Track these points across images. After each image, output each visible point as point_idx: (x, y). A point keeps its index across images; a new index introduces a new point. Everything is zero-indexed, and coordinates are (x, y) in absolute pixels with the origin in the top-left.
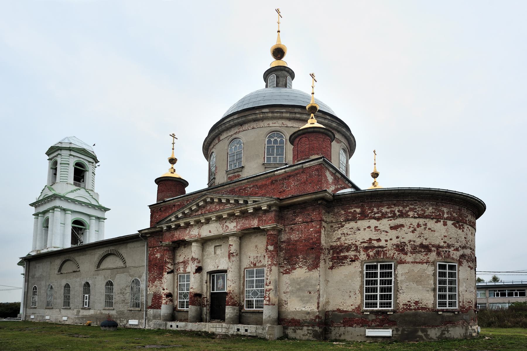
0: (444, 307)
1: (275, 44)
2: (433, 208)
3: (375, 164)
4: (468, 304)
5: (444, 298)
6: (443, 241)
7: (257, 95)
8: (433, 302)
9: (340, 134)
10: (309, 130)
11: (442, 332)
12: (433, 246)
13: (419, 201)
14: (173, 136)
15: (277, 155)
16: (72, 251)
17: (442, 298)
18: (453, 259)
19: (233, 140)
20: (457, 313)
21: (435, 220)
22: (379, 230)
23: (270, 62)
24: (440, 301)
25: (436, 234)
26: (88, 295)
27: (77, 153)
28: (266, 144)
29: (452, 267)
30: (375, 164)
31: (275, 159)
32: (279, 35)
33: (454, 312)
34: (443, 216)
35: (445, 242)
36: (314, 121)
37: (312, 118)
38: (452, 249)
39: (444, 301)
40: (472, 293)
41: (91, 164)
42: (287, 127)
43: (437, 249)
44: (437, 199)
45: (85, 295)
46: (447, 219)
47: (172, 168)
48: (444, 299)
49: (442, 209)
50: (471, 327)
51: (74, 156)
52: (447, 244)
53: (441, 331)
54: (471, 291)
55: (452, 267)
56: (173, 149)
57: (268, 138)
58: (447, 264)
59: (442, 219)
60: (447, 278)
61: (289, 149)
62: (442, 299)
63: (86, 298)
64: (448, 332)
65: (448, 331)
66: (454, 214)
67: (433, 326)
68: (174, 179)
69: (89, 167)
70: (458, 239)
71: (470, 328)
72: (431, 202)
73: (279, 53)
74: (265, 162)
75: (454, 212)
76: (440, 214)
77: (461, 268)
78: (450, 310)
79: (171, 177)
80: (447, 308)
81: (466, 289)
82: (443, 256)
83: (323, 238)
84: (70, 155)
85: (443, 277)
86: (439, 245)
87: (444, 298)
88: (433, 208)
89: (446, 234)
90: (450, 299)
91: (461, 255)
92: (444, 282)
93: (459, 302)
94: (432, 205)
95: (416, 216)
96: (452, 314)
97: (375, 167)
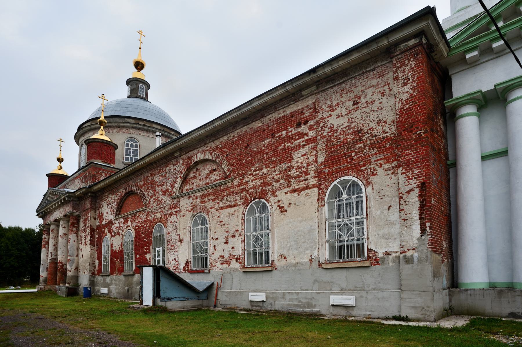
7: (119, 104)
14: (61, 140)
15: (133, 156)
16: (504, 28)
22: (190, 211)
26: (161, 249)
31: (132, 159)
32: (140, 51)
45: (157, 249)
63: (159, 254)
73: (139, 66)
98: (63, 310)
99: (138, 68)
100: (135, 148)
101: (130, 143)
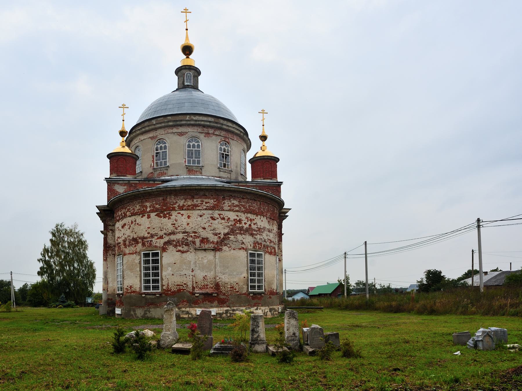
0: (157, 290)
2: (139, 206)
3: (263, 125)
5: (157, 282)
6: (147, 232)
7: (164, 102)
8: (139, 286)
9: (184, 127)
10: (119, 154)
11: (145, 312)
12: (140, 238)
13: (131, 202)
17: (156, 282)
18: (156, 247)
20: (158, 295)
21: (141, 215)
25: (142, 227)
29: (156, 254)
30: (263, 125)
33: (155, 295)
34: (146, 210)
35: (148, 233)
38: (156, 237)
39: (157, 285)
42: (141, 141)
43: (143, 241)
44: (140, 198)
46: (150, 212)
49: (146, 205)
52: (151, 234)
53: (144, 311)
58: (151, 252)
59: (146, 213)
60: (151, 265)
62: (156, 283)
64: (149, 312)
65: (149, 312)
66: (157, 206)
67: (140, 307)
68: (261, 158)
70: (162, 227)
72: (138, 201)
73: (187, 50)
74: (155, 167)
75: (157, 204)
76: (144, 209)
77: (164, 254)
80: (151, 291)
81: (172, 273)
82: (147, 246)
83: (111, 239)
86: (144, 237)
87: (157, 282)
88: (139, 206)
89: (149, 226)
91: (165, 242)
93: (162, 286)
94: (139, 203)
95: (130, 215)
96: (154, 297)
97: (263, 129)
98: (292, 342)
99: (187, 53)
100: (197, 148)
101: (191, 144)
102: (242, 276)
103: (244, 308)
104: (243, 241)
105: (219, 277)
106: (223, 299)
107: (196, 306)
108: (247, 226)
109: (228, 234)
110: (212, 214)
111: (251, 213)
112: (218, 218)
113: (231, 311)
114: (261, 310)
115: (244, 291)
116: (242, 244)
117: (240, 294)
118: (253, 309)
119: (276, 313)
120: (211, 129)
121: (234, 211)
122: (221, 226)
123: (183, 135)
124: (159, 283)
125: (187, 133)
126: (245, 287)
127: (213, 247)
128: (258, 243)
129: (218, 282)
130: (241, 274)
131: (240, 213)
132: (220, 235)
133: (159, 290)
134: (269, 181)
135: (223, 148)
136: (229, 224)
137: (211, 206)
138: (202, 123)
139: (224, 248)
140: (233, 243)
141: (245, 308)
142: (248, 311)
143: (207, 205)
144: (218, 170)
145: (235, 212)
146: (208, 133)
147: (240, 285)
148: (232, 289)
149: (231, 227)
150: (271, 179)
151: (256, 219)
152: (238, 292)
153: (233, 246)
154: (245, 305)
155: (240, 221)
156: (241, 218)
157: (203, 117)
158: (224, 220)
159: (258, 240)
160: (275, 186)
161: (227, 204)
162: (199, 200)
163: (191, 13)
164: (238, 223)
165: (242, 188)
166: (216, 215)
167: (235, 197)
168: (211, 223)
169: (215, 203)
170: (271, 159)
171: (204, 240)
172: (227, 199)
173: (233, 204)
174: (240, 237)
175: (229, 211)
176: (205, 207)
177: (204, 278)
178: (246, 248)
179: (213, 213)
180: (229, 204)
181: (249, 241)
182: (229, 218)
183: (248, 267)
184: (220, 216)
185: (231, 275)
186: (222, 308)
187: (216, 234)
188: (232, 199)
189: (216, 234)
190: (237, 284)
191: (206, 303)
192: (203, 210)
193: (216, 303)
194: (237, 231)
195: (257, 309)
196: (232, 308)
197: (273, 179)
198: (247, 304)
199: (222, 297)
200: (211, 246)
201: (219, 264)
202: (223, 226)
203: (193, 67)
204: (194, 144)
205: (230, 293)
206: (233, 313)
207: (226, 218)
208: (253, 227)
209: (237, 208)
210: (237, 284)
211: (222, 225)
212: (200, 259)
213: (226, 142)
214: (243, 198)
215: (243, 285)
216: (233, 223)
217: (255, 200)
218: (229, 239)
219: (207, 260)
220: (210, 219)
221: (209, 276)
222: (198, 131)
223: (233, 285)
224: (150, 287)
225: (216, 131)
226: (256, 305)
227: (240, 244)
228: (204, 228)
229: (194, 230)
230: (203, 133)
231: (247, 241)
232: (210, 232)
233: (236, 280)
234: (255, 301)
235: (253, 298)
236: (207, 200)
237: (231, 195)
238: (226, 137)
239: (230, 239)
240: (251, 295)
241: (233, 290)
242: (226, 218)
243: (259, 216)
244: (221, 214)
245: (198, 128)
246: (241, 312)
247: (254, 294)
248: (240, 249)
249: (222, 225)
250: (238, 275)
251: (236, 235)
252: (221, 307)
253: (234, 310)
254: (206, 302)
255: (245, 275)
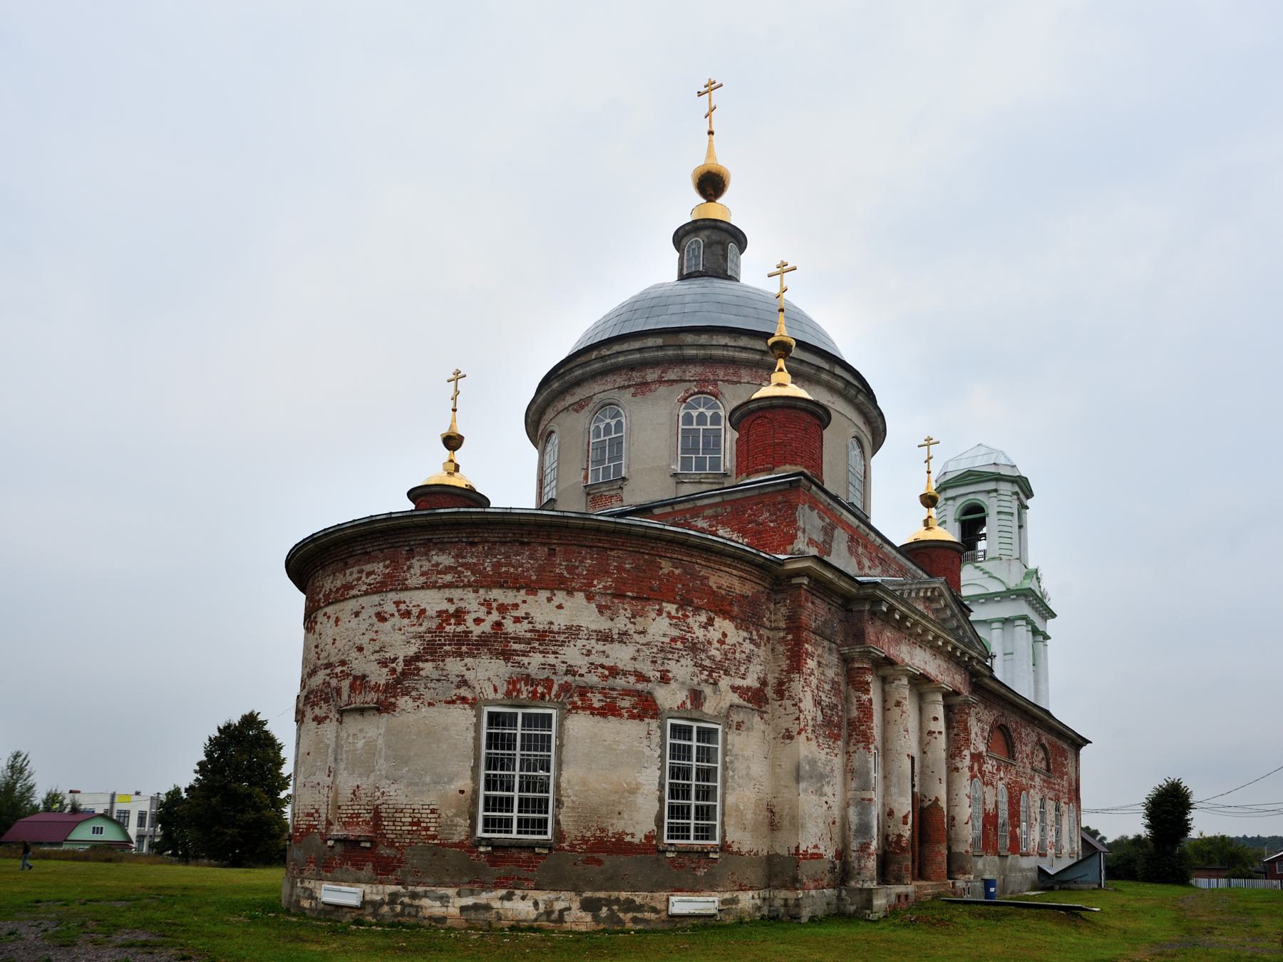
1: (702, 163)
4: (305, 818)
17: (678, 813)
19: (602, 407)
23: (688, 205)
24: (673, 823)
27: (958, 489)
28: (723, 429)
29: (706, 735)
36: (785, 377)
37: (781, 370)
40: (318, 788)
41: (994, 494)
47: (451, 461)
48: (683, 818)
50: (302, 882)
51: (953, 498)
54: (316, 782)
55: (706, 735)
56: (454, 410)
57: (684, 409)
60: (694, 763)
61: (729, 437)
62: (678, 818)
69: (991, 506)
71: (299, 885)
73: (711, 184)
78: (696, 847)
79: (937, 541)
84: (947, 499)
85: (684, 760)
90: (673, 818)
92: (507, 763)
102: (452, 787)
103: (451, 892)
104: (466, 677)
105: (382, 790)
106: (388, 857)
107: (329, 875)
108: (486, 627)
109: (417, 658)
110: (380, 605)
111: (501, 587)
112: (392, 615)
113: (404, 896)
114: (531, 903)
115: (460, 834)
116: (458, 687)
117: (444, 845)
118: (489, 897)
119: (409, 913)
120: (651, 370)
121: (440, 588)
122: (398, 638)
123: (582, 407)
124: (546, 812)
125: (590, 398)
126: (463, 823)
127: (375, 700)
128: (528, 679)
129: (378, 805)
130: (451, 780)
131: (460, 591)
132: (394, 665)
133: (546, 833)
134: (762, 478)
135: (695, 413)
136: (422, 629)
137: (377, 583)
138: (621, 359)
139: (404, 702)
140: (429, 685)
141: (457, 890)
142: (469, 901)
143: (368, 581)
144: (672, 481)
145: (442, 590)
146: (646, 384)
147: (443, 815)
148: (415, 828)
149: (428, 637)
150: (770, 471)
151: (524, 602)
152: (434, 837)
153: (428, 695)
154: (456, 880)
155: (459, 615)
156: (462, 604)
157: (632, 343)
158: (409, 618)
159: (533, 670)
160: (780, 491)
161: (417, 569)
162: (355, 569)
163: (721, 86)
164: (453, 621)
165: (447, 510)
166: (389, 608)
167: (443, 543)
168: (377, 632)
169: (387, 571)
170: (772, 407)
171: (360, 682)
172: (419, 553)
173: (438, 564)
174: (454, 666)
175: (422, 588)
176: (364, 588)
177: (354, 793)
178: (474, 699)
179: (382, 602)
180: (425, 569)
181: (491, 674)
182: (423, 611)
183: (477, 759)
184: (397, 606)
185: (416, 784)
186: (381, 887)
187: (385, 663)
188: (434, 553)
189: (383, 663)
190: (433, 811)
191: (348, 869)
192: (361, 595)
193: (368, 869)
194: (447, 648)
195: (509, 897)
196: (410, 888)
197: (776, 469)
198: (466, 879)
199: (384, 851)
200: (372, 697)
201: (384, 750)
202: (404, 637)
203: (702, 223)
204: (608, 424)
205: (408, 841)
206: (411, 906)
207: (415, 611)
208: (510, 630)
209: (449, 578)
210: (433, 811)
211: (402, 632)
212: (351, 740)
213: (707, 393)
214: (473, 544)
215: (456, 815)
216: (434, 624)
217: (522, 543)
218: (418, 674)
219: (363, 741)
220: (375, 619)
221: (365, 786)
222: (616, 386)
223: (419, 815)
224: (508, 822)
225: (670, 372)
226: (510, 885)
227: (453, 686)
228: (360, 649)
229: (343, 657)
230: (629, 386)
231: (482, 674)
232: (373, 658)
233: (431, 799)
234: (502, 871)
235: (493, 860)
236: (368, 568)
237: (429, 540)
238: (704, 381)
239: (421, 673)
240: (482, 849)
241: (417, 830)
242: (415, 611)
243: (543, 595)
244: (400, 602)
245: (615, 377)
246: (438, 904)
247: (493, 847)
248: (453, 702)
249: (402, 632)
250: (438, 783)
251: (443, 661)
252: (381, 883)
253: (414, 896)
254: (347, 864)
255: (465, 783)
